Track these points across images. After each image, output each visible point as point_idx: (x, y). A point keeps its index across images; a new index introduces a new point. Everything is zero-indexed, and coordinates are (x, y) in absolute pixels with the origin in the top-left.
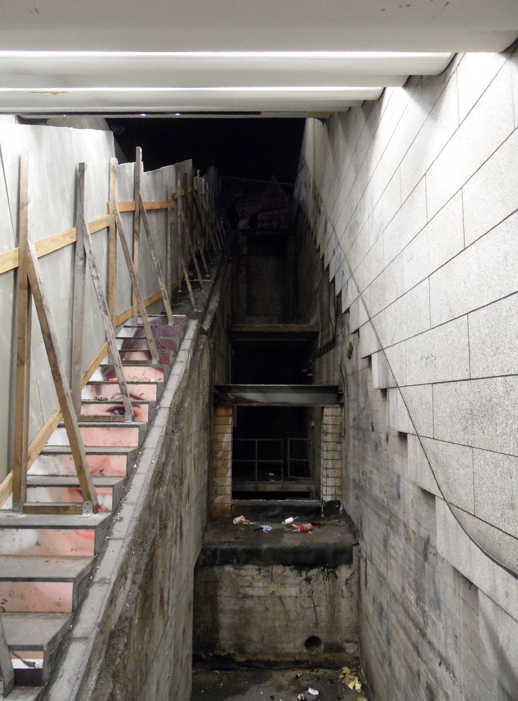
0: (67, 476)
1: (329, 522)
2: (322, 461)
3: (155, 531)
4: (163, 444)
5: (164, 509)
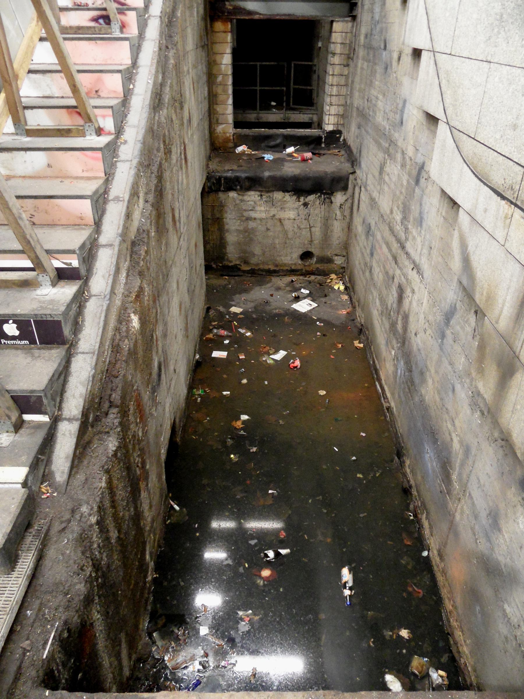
0: (63, 97)
1: (329, 152)
2: (327, 87)
3: (160, 154)
4: (158, 62)
5: (167, 133)
